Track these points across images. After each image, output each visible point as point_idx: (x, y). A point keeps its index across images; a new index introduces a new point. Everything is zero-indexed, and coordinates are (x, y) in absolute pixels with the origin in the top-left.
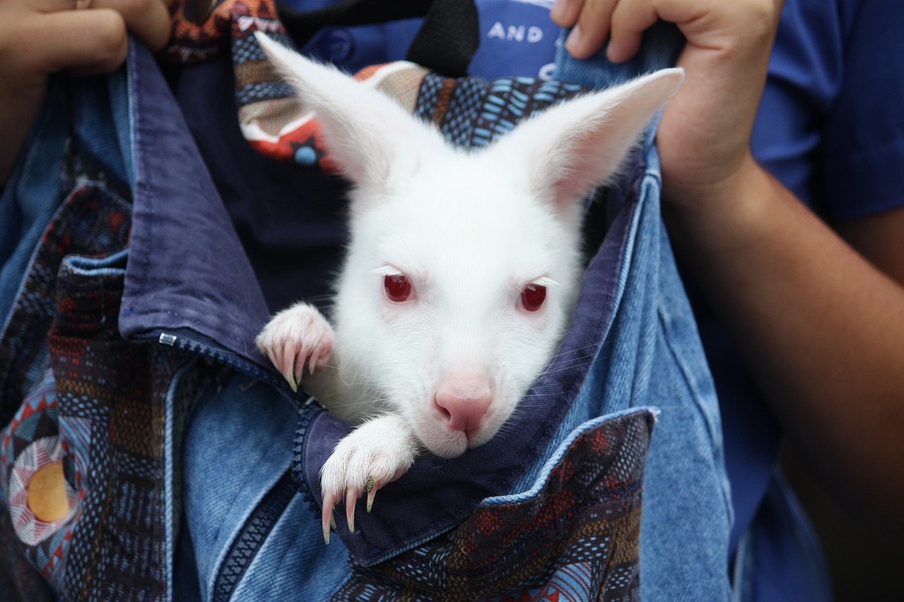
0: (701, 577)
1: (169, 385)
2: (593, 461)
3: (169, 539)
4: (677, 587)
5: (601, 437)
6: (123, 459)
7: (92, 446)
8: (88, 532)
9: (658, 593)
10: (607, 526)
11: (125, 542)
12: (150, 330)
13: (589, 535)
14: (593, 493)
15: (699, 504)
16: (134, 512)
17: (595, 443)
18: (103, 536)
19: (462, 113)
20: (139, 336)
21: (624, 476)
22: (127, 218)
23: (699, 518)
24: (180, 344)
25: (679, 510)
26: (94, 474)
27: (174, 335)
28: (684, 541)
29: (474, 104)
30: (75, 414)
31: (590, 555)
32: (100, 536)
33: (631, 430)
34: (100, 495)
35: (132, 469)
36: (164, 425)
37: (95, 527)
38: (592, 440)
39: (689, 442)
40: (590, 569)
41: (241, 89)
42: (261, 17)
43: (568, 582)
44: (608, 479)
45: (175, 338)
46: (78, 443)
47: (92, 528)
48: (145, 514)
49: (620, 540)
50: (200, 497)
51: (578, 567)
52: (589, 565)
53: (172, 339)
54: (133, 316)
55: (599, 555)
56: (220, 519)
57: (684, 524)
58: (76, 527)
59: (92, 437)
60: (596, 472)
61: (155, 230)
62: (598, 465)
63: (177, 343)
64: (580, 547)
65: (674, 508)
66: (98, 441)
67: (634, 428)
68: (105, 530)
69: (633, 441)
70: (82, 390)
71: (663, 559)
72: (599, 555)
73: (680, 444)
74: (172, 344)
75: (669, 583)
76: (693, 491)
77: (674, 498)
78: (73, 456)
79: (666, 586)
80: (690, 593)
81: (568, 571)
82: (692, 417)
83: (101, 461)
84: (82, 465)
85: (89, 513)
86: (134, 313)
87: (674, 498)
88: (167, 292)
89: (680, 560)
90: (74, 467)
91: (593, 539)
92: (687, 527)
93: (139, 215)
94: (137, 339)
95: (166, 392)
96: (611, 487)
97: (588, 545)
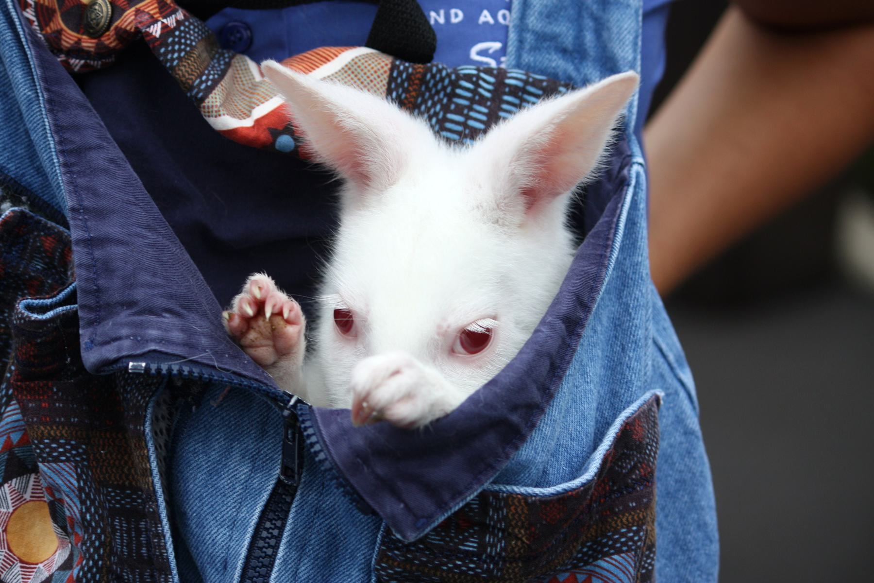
0: (703, 545)
1: (145, 416)
2: (632, 450)
4: (682, 558)
5: (639, 425)
6: (109, 493)
8: (94, 576)
9: (666, 565)
12: (117, 360)
13: (630, 525)
14: (630, 481)
15: (694, 474)
16: (129, 546)
17: (635, 432)
18: (108, 578)
19: (431, 97)
20: (106, 368)
22: (65, 245)
23: (696, 488)
24: (151, 369)
26: (88, 517)
27: (142, 361)
28: (684, 512)
29: (444, 88)
30: (56, 460)
31: (633, 545)
32: (105, 578)
34: (98, 537)
35: (118, 502)
36: (148, 458)
37: (99, 570)
38: (633, 428)
39: (677, 416)
40: (633, 558)
41: (191, 88)
42: (165, 17)
43: (615, 573)
44: (643, 468)
45: (144, 364)
46: (64, 488)
47: (97, 572)
48: (139, 546)
50: (201, 526)
51: (623, 558)
52: (632, 555)
53: (141, 366)
54: (95, 348)
56: (225, 547)
57: (683, 496)
58: (79, 572)
60: (633, 460)
61: (98, 253)
62: (635, 453)
63: (147, 369)
64: (623, 538)
65: (672, 482)
66: (85, 484)
68: (110, 571)
70: (58, 433)
71: (667, 532)
73: (671, 419)
74: (143, 372)
75: (676, 555)
76: (688, 463)
77: (671, 472)
78: (61, 501)
79: (673, 558)
80: (695, 562)
81: (614, 562)
82: (676, 393)
83: (93, 502)
84: (73, 508)
85: (91, 557)
86: (96, 346)
87: (671, 472)
88: (124, 316)
89: (683, 530)
90: (64, 512)
91: (634, 528)
92: (686, 498)
93: (78, 242)
94: (104, 371)
95: (144, 425)
96: (645, 475)
97: (631, 534)
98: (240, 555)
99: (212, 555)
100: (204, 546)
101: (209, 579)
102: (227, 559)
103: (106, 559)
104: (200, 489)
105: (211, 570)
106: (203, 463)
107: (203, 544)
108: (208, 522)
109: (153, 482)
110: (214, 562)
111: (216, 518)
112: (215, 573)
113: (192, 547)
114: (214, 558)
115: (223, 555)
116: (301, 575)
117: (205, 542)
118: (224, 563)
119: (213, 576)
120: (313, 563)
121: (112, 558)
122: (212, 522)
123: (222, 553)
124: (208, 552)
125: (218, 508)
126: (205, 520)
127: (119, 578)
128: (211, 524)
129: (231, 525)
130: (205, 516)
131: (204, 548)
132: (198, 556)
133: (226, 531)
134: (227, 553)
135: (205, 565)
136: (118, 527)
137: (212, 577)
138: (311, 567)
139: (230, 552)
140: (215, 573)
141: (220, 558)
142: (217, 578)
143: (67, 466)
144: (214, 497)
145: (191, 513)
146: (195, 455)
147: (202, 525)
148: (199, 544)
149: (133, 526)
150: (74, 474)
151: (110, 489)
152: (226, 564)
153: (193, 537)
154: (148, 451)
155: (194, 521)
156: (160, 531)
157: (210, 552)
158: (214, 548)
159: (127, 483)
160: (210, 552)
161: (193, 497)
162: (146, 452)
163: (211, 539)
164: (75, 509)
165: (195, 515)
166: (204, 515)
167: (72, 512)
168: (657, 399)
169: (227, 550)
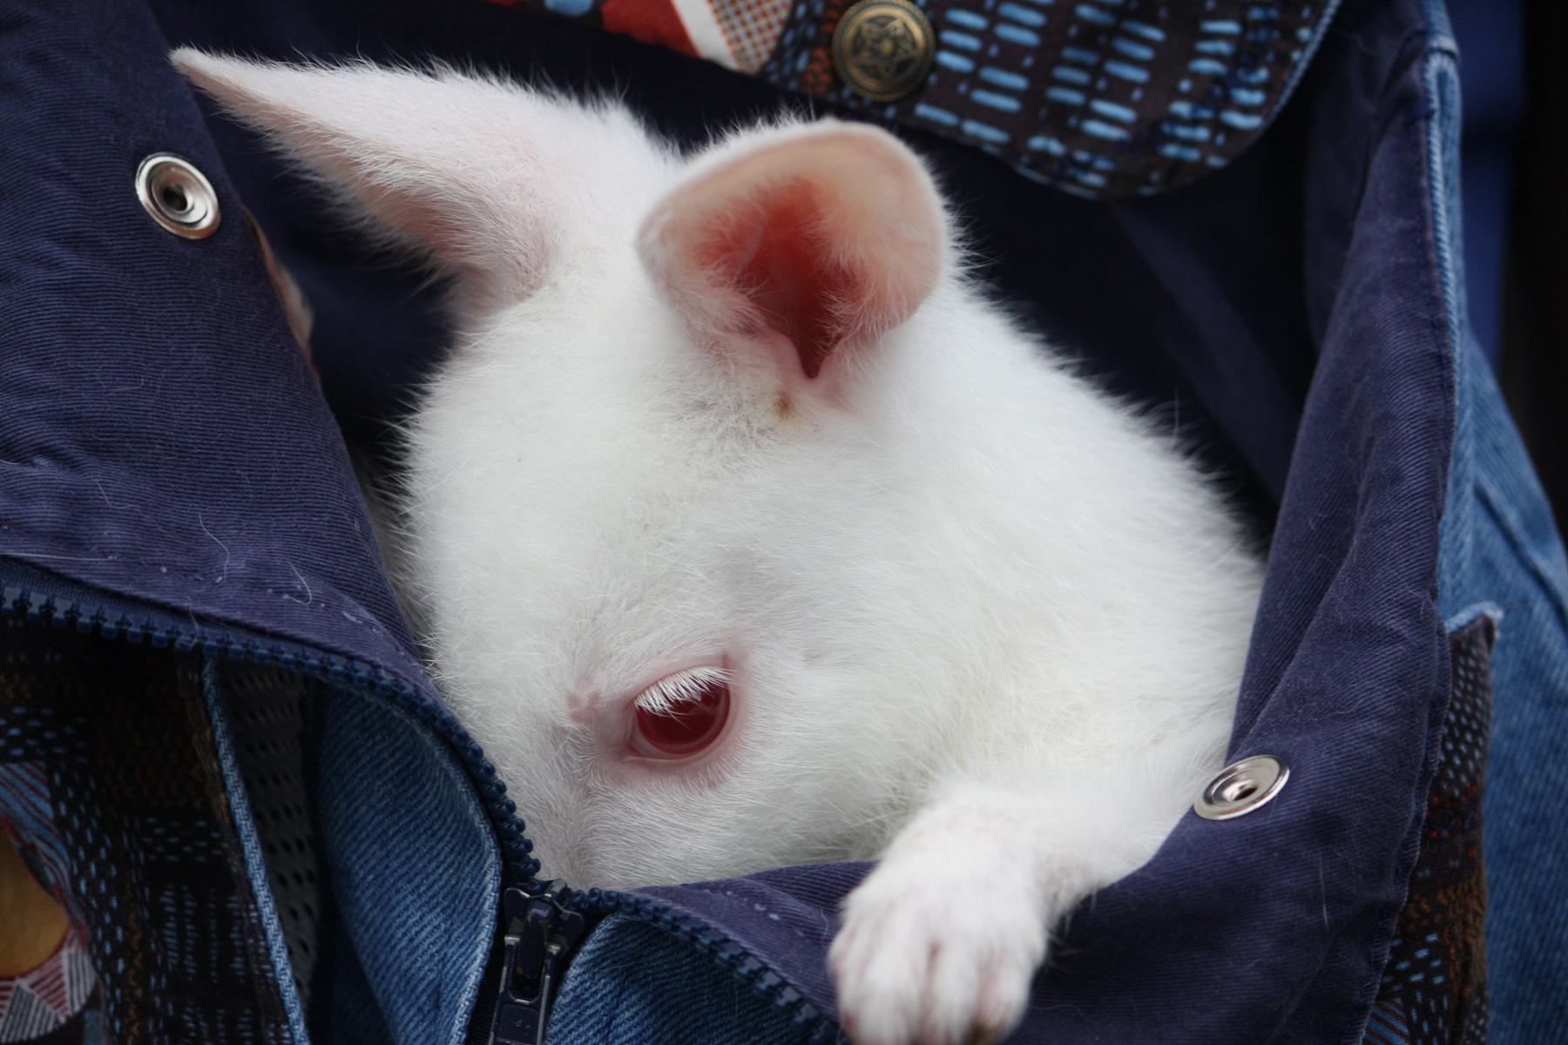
3: (296, 1014)
7: (61, 823)
10: (1425, 906)
11: (198, 1029)
21: (1457, 782)
25: (1523, 825)
33: (1466, 668)
49: (1474, 932)
52: (1398, 1006)
55: (1417, 978)
59: (54, 803)
66: (72, 806)
67: (1472, 663)
69: (1474, 695)
72: (1417, 978)
78: (33, 847)
95: (201, 669)
98: (466, 979)
99: (408, 975)
100: (391, 952)
101: (404, 1030)
102: (440, 985)
103: (133, 983)
104: (381, 817)
105: (408, 1011)
106: (386, 755)
107: (388, 949)
108: (401, 896)
109: (228, 806)
110: (413, 991)
111: (418, 887)
112: (416, 1019)
113: (363, 952)
114: (413, 983)
115: (432, 976)
116: (621, 1029)
117: (393, 943)
118: (435, 996)
119: (412, 1025)
120: (652, 1002)
121: (153, 980)
122: (411, 898)
123: (431, 970)
124: (399, 967)
125: (420, 865)
126: (394, 890)
127: (175, 1028)
128: (408, 901)
129: (449, 907)
130: (394, 883)
131: (391, 959)
132: (376, 975)
133: (440, 919)
134: (440, 972)
135: (394, 996)
136: (169, 909)
137: (408, 1024)
138: (647, 1012)
139: (446, 970)
140: (416, 1019)
141: (426, 982)
142: (420, 1028)
143: (28, 771)
144: (412, 838)
145: (362, 873)
146: (366, 735)
147: (387, 904)
148: (379, 948)
149: (212, 906)
150: (44, 789)
151: (151, 820)
152: (438, 999)
153: (367, 930)
154: (213, 732)
155: (369, 893)
156: (254, 921)
157: (404, 967)
158: (412, 959)
159: (198, 804)
160: (404, 967)
161: (367, 836)
162: (208, 733)
163: (407, 938)
164: (62, 865)
165: (371, 877)
166: (392, 880)
167: (58, 874)
168: (1488, 627)
169: (440, 965)
